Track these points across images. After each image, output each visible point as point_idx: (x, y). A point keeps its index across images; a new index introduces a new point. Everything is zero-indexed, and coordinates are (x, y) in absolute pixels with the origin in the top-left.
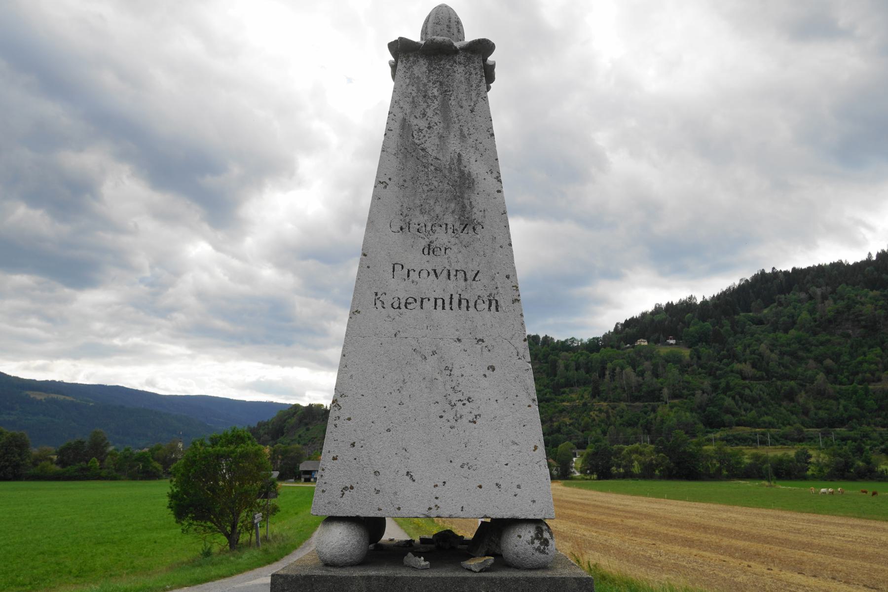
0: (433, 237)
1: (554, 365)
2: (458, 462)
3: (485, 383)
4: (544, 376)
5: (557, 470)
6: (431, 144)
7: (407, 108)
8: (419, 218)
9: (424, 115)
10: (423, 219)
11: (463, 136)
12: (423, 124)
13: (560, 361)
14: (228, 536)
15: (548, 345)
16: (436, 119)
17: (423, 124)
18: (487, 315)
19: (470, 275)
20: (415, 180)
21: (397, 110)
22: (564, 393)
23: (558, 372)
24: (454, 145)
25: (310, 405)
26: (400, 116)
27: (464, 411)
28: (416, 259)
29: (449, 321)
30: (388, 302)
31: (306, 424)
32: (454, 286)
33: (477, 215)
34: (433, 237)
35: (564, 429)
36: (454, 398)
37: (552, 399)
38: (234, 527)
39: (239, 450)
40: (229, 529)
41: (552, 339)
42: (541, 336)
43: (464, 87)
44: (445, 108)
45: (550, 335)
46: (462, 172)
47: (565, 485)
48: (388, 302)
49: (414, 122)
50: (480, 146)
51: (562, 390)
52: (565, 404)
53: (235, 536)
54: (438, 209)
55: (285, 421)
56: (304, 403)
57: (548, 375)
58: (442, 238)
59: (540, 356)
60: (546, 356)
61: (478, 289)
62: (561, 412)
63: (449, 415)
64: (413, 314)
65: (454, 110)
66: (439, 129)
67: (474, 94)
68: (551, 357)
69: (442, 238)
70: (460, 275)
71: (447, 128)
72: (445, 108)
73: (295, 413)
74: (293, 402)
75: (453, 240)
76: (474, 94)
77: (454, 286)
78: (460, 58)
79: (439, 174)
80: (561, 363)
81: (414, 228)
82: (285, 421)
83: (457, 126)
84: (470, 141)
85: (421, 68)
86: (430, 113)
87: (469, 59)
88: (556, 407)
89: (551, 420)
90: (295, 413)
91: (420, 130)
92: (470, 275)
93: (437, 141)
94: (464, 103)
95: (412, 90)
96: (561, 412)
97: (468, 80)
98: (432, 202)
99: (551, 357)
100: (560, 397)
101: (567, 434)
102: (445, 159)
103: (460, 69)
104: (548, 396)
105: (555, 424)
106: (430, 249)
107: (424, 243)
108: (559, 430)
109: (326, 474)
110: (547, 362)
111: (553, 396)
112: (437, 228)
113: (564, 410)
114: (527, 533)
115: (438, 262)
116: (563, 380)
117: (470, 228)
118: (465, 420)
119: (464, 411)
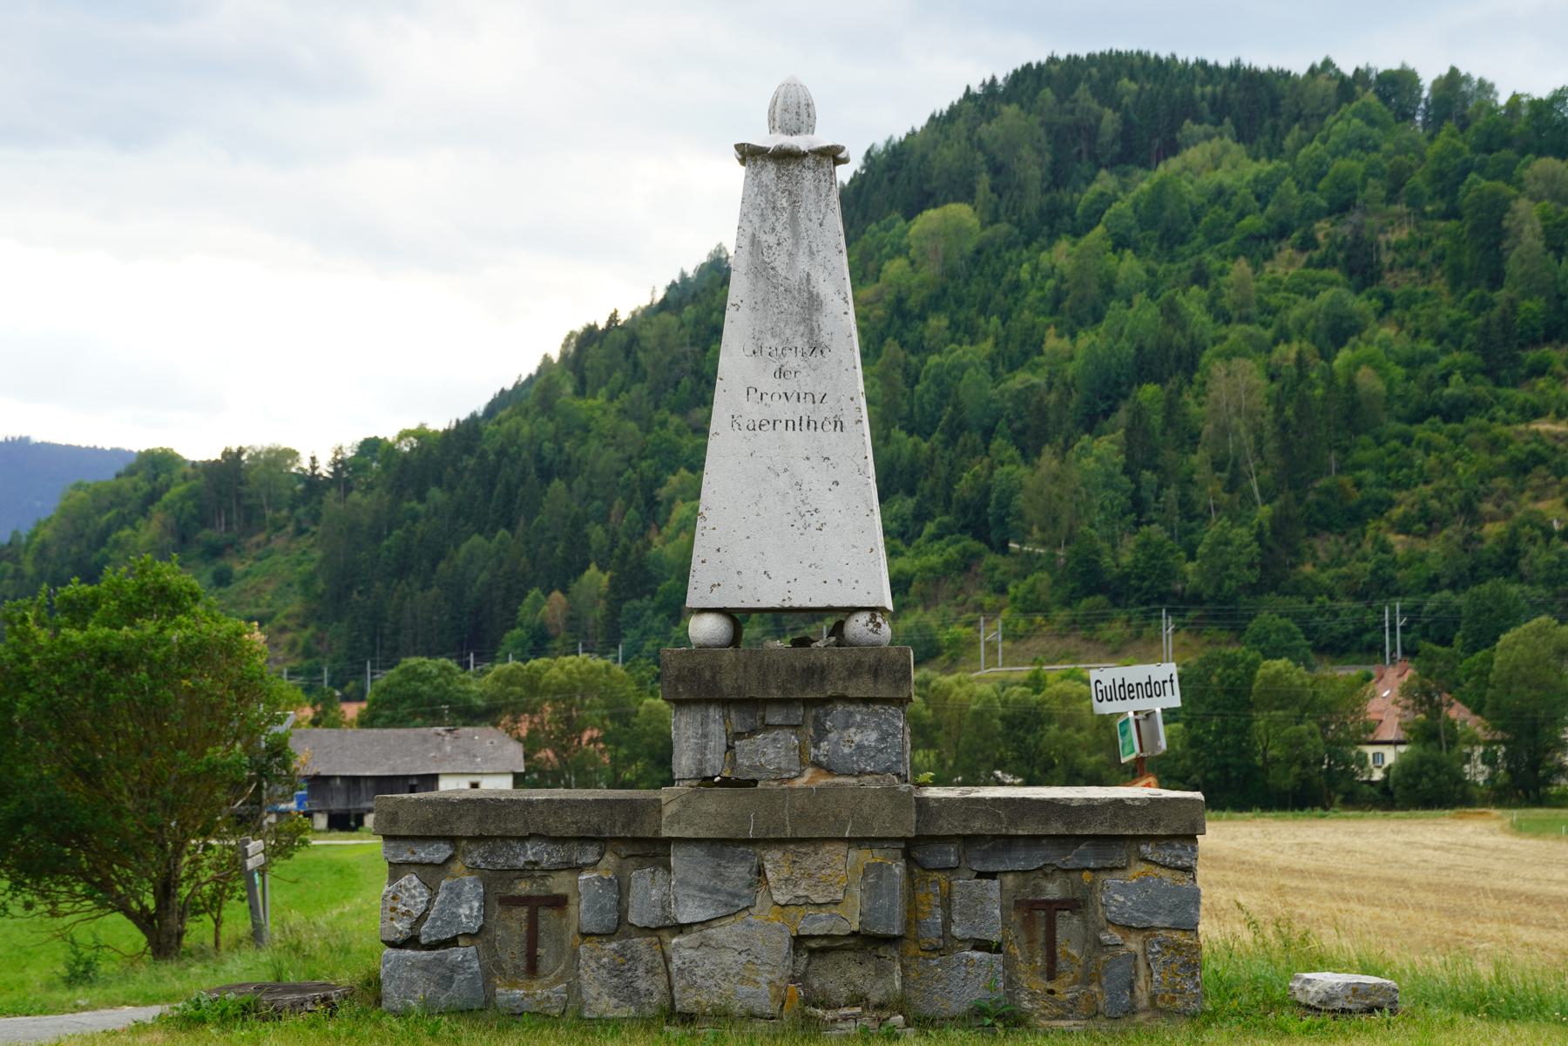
0: (783, 361)
1: (1491, 229)
2: (806, 563)
3: (830, 496)
4: (1440, 285)
5: (1489, 759)
6: (780, 263)
7: (756, 220)
8: (770, 342)
9: (773, 229)
10: (774, 342)
11: (812, 253)
12: (772, 240)
13: (1522, 205)
14: (143, 920)
15: (1464, 124)
16: (786, 234)
17: (772, 240)
18: (833, 435)
19: (818, 398)
20: (765, 301)
21: (746, 225)
22: (1539, 370)
23: (1512, 266)
24: (803, 263)
25: (233, 458)
26: (749, 231)
27: (812, 520)
28: (768, 383)
29: (799, 440)
30: (743, 422)
31: (215, 552)
32: (804, 409)
33: (824, 338)
34: (783, 361)
35: (1538, 557)
36: (803, 509)
37: (1477, 405)
38: (165, 890)
39: (175, 635)
40: (150, 902)
41: (1485, 88)
42: (1429, 74)
43: (813, 196)
44: (794, 221)
45: (1474, 67)
46: (810, 293)
47: (1518, 829)
48: (743, 422)
49: (763, 237)
50: (829, 265)
51: (1531, 355)
52: (1543, 426)
53: (172, 921)
54: (788, 332)
55: (103, 537)
56: (200, 446)
57: (1457, 278)
58: (792, 361)
59: (1418, 180)
60: (1448, 181)
61: (825, 411)
62: (1521, 468)
63: (800, 524)
64: (767, 434)
65: (804, 224)
66: (788, 245)
67: (823, 204)
68: (1478, 185)
69: (792, 361)
70: (809, 397)
71: (796, 244)
72: (794, 221)
73: (153, 497)
74: (138, 439)
75: (803, 364)
76: (823, 204)
77: (804, 409)
78: (809, 162)
79: (789, 296)
80: (1527, 218)
81: (766, 351)
82: (103, 537)
83: (806, 242)
84: (819, 258)
85: (770, 172)
86: (779, 228)
87: (818, 163)
88: (1495, 445)
89: (1468, 510)
90: (153, 497)
91: (770, 247)
92: (818, 398)
93: (786, 259)
94: (814, 216)
95: (761, 200)
96: (1521, 468)
97: (817, 188)
98: (782, 325)
99: (1478, 185)
100: (1520, 395)
101: (1550, 582)
102: (795, 280)
103: (809, 175)
104: (1456, 387)
105: (1492, 529)
106: (781, 373)
107: (775, 367)
108: (1508, 561)
109: (697, 575)
110: (1452, 214)
111: (1483, 388)
112: (787, 352)
113: (1537, 459)
114: (864, 618)
115: (789, 385)
116: (1533, 305)
117: (818, 351)
118: (812, 528)
119: (812, 520)
